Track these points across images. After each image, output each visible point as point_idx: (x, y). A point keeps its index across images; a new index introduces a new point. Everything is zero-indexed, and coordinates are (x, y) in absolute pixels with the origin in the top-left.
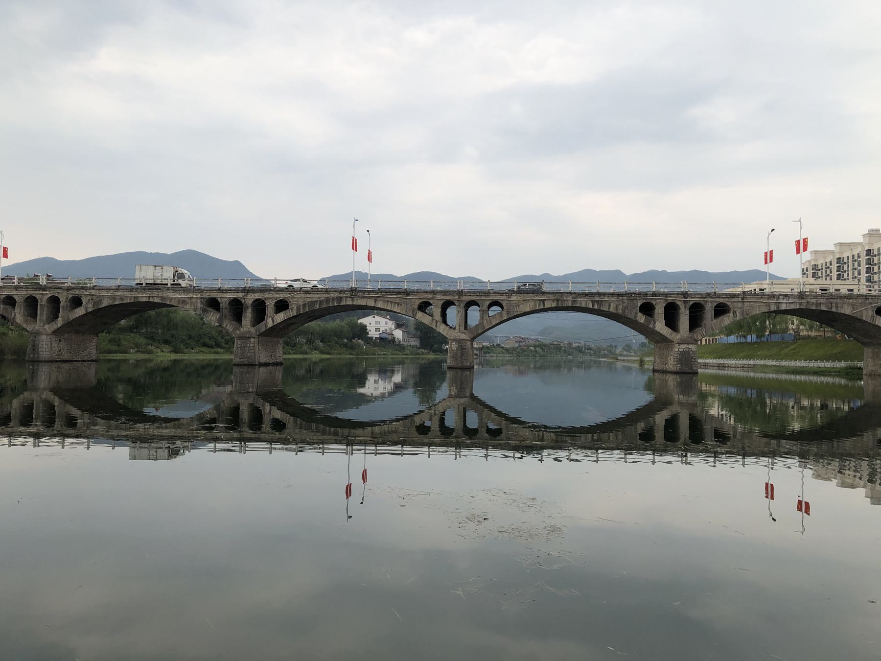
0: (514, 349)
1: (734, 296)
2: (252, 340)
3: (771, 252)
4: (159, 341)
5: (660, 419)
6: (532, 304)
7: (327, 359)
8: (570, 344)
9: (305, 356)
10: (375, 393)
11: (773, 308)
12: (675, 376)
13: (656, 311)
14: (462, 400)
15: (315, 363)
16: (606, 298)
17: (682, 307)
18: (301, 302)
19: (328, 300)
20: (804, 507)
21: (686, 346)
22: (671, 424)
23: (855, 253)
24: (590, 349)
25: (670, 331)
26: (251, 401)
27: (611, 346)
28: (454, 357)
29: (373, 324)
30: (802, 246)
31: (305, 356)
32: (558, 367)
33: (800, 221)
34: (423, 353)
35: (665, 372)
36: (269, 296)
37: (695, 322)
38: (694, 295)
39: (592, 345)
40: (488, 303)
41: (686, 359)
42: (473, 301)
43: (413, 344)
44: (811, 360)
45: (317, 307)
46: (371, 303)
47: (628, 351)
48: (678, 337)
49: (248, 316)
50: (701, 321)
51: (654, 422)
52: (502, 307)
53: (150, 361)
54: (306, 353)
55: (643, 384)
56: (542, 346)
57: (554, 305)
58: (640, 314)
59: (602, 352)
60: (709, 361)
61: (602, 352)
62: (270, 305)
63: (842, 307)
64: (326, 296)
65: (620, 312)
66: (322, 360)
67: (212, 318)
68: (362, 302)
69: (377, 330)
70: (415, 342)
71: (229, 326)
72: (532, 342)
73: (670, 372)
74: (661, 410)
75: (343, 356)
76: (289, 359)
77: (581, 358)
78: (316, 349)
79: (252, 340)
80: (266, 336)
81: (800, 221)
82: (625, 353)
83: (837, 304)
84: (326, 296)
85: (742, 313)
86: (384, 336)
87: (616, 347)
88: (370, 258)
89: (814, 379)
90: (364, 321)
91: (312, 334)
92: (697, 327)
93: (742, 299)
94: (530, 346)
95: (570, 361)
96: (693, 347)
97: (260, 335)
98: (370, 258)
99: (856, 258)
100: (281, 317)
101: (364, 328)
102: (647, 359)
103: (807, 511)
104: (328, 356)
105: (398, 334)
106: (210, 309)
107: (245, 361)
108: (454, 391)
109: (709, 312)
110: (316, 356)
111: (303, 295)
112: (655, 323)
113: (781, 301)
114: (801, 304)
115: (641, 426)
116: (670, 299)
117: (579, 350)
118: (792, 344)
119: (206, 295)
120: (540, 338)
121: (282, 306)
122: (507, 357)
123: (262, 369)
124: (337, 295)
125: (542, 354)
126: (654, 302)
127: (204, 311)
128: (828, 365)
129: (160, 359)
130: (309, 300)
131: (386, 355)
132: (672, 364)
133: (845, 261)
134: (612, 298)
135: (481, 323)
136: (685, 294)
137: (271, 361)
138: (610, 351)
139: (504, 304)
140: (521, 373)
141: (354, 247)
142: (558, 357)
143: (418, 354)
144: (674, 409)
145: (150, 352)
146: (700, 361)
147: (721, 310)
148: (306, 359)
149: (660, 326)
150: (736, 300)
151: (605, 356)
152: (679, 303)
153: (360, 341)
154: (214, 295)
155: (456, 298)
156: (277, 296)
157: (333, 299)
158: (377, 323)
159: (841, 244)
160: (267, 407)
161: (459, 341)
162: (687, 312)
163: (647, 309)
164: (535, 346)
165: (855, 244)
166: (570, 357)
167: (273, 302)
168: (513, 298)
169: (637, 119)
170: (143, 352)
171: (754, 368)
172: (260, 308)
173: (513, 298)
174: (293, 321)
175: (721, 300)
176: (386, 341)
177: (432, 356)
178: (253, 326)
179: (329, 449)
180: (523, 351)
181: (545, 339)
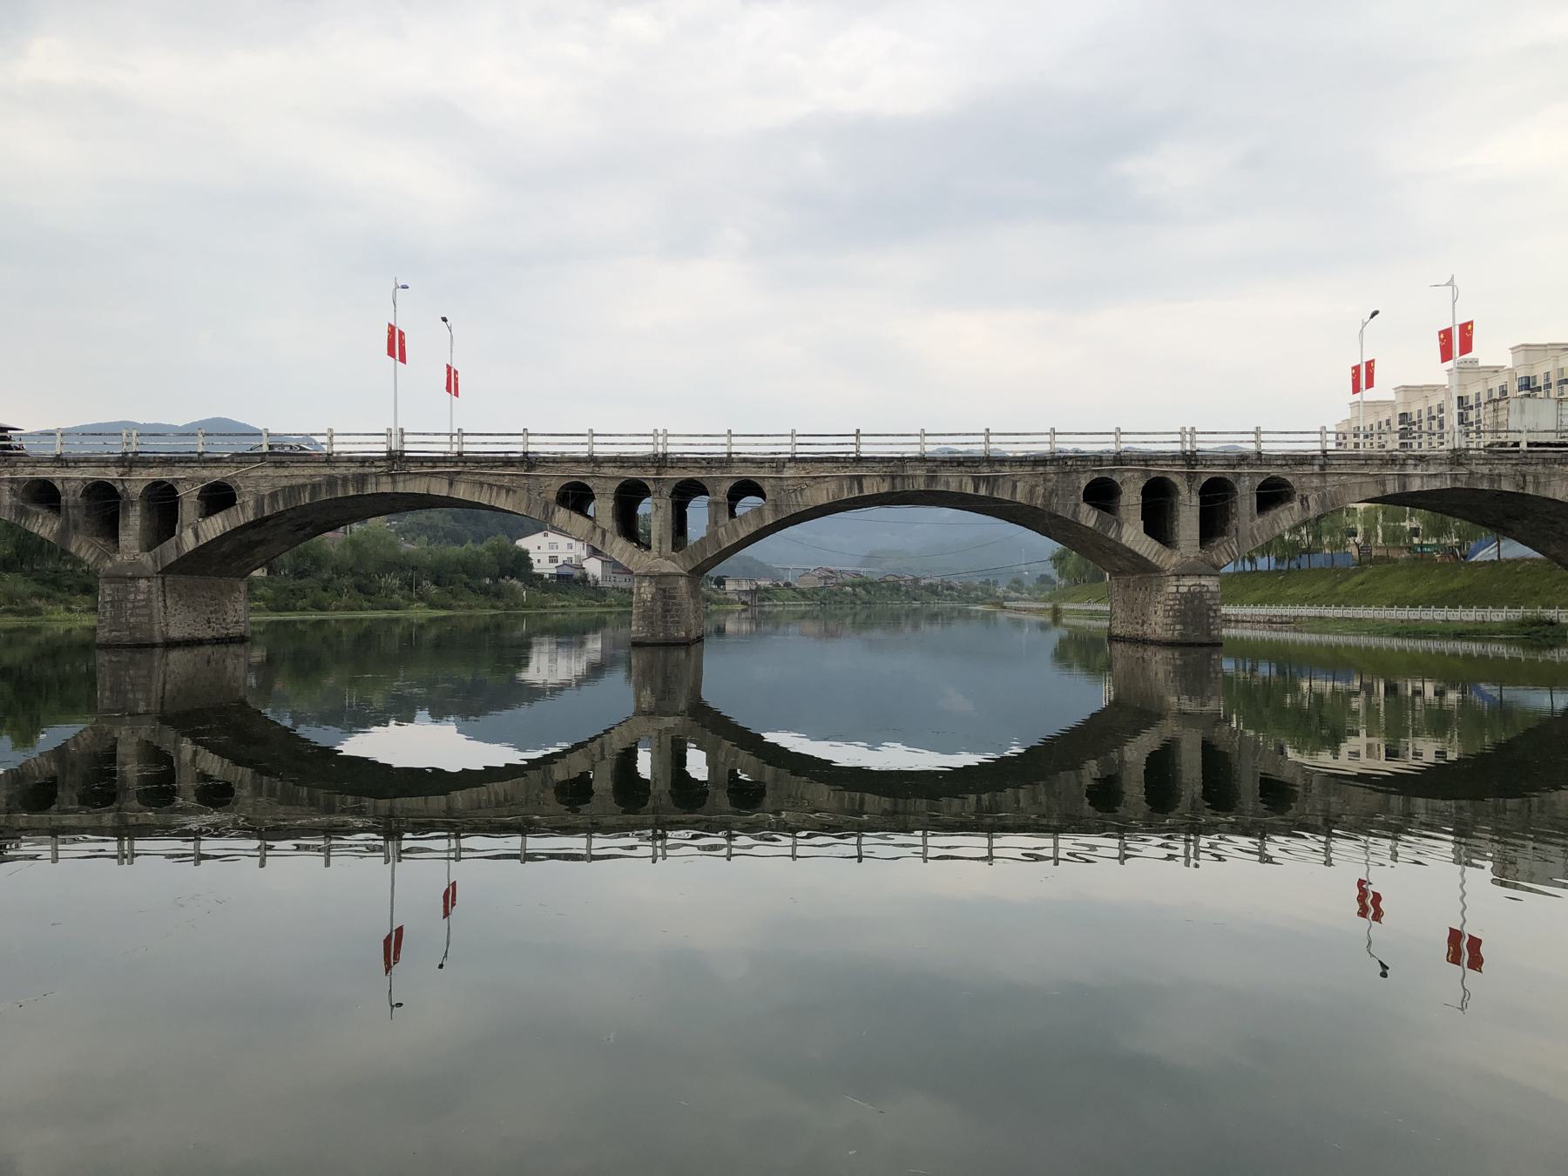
0: (815, 591)
1: (1301, 460)
2: (143, 584)
3: (1370, 365)
4: (70, 587)
5: (1136, 752)
6: (833, 486)
7: (444, 619)
8: (916, 580)
10: (553, 680)
11: (1392, 488)
12: (1168, 653)
13: (1124, 500)
14: (669, 722)
15: (421, 627)
16: (1006, 470)
17: (1183, 488)
18: (265, 489)
19: (331, 482)
20: (1464, 950)
21: (1195, 581)
22: (1161, 765)
23: (1434, 403)
24: (951, 588)
25: (1156, 545)
26: (144, 732)
27: (987, 582)
28: (647, 617)
29: (545, 548)
30: (1456, 341)
32: (895, 620)
33: (1451, 283)
35: (1143, 642)
36: (188, 473)
37: (1213, 524)
39: (955, 583)
40: (727, 485)
41: (1195, 610)
42: (691, 481)
44: (1402, 606)
45: (306, 499)
46: (440, 488)
47: (1017, 590)
48: (1174, 560)
49: (133, 524)
50: (1226, 521)
51: (1122, 762)
52: (760, 493)
53: (35, 630)
55: (1051, 650)
56: (866, 585)
57: (885, 488)
58: (1085, 507)
62: (189, 496)
63: (1548, 484)
64: (328, 471)
65: (1039, 503)
66: (432, 621)
67: (44, 526)
68: (418, 487)
69: (553, 559)
71: (84, 549)
72: (848, 579)
74: (1137, 733)
75: (477, 612)
76: (1302, 601)
77: (936, 605)
78: (421, 599)
79: (143, 584)
80: (181, 572)
81: (1451, 283)
82: (1013, 594)
83: (1536, 477)
84: (328, 471)
85: (1321, 502)
86: (566, 570)
87: (996, 583)
88: (452, 385)
89: (1449, 646)
90: (523, 543)
91: (414, 568)
92: (1223, 533)
93: (1322, 467)
96: (1211, 583)
97: (167, 570)
98: (452, 385)
99: (1435, 413)
100: (215, 526)
101: (523, 558)
102: (1065, 606)
103: (1476, 962)
104: (443, 613)
105: (594, 567)
106: (33, 508)
107: (125, 636)
108: (647, 699)
109: (1245, 500)
110: (418, 613)
111: (270, 471)
112: (1120, 526)
113: (1410, 470)
114: (1455, 478)
115: (1092, 770)
116: (1156, 471)
117: (932, 590)
118: (1356, 572)
119: (25, 473)
120: (862, 570)
121: (218, 498)
122: (803, 606)
123: (175, 655)
124: (355, 470)
125: (866, 598)
126: (1116, 478)
127: (22, 512)
128: (1472, 615)
129: (61, 628)
130: (285, 482)
131: (567, 608)
132: (1159, 623)
133: (1415, 418)
134: (1019, 470)
135: (712, 535)
137: (209, 634)
139: (766, 489)
140: (830, 635)
141: (396, 345)
142: (896, 605)
145: (36, 612)
146: (1224, 610)
147: (1272, 494)
148: (397, 621)
149: (1133, 535)
150: (1307, 469)
151: (977, 601)
152: (1175, 479)
153: (514, 582)
154: (44, 473)
156: (205, 473)
157: (345, 479)
158: (552, 545)
159: (1406, 388)
160: (187, 747)
161: (658, 578)
162: (1196, 500)
163: (1102, 494)
164: (853, 586)
165: (1434, 388)
166: (916, 604)
167: (195, 491)
168: (787, 473)
169: (1022, 171)
170: (19, 613)
171: (1294, 623)
172: (163, 501)
173: (787, 473)
174: (254, 535)
175: (1274, 471)
176: (569, 581)
178: (149, 548)
179: (338, 846)
181: (873, 572)
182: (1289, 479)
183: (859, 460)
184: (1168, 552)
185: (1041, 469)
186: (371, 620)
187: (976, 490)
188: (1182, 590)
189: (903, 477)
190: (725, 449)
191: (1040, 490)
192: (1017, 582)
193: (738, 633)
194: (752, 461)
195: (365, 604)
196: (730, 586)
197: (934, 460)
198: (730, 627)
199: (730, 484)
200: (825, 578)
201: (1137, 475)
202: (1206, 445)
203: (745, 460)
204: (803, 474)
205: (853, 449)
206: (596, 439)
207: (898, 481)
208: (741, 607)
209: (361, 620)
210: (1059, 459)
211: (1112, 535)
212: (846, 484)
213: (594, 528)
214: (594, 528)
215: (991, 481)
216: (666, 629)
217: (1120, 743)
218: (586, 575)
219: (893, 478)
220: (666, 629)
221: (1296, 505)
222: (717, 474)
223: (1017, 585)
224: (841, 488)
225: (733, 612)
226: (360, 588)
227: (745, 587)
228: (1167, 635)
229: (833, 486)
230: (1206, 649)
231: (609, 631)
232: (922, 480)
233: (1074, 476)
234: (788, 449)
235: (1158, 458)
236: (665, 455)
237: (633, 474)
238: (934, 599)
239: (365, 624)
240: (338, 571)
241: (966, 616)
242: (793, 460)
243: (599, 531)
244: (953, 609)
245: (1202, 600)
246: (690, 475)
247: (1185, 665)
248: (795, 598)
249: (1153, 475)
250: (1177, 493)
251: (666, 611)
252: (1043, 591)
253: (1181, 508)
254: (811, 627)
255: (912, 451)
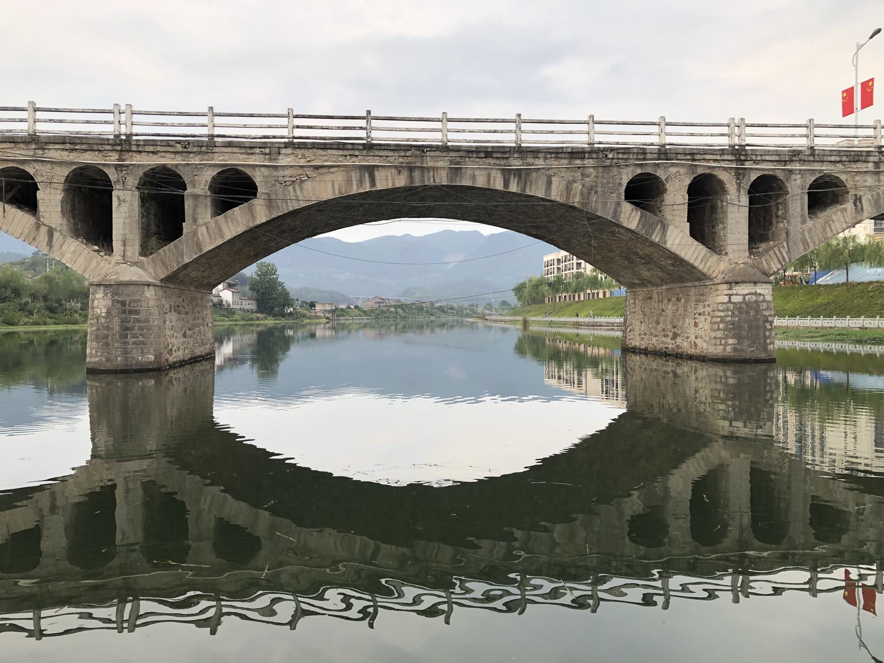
0: (373, 311)
1: (857, 157)
8: (432, 304)
9: (76, 327)
12: (719, 371)
16: (540, 163)
22: (707, 489)
24: (452, 308)
27: (472, 305)
31: (76, 327)
32: (421, 327)
34: (258, 319)
37: (760, 230)
38: (759, 155)
39: (455, 305)
41: (748, 322)
43: (248, 307)
44: (783, 316)
51: (666, 489)
54: (75, 323)
55: (513, 346)
56: (403, 306)
58: (627, 207)
59: (465, 312)
60: (553, 319)
61: (465, 312)
65: (576, 201)
70: (251, 305)
72: (393, 303)
73: (703, 359)
77: (443, 318)
82: (487, 312)
94: (391, 306)
95: (432, 321)
96: (765, 291)
112: (664, 228)
117: (442, 309)
122: (365, 320)
125: (403, 315)
126: (661, 174)
134: (554, 163)
136: (739, 153)
138: (472, 310)
142: (421, 319)
143: (252, 319)
144: (718, 453)
147: (824, 195)
149: (678, 238)
150: (862, 167)
151: (467, 316)
152: (723, 176)
155: (113, 158)
161: (115, 288)
162: (745, 200)
163: (644, 192)
164: (396, 307)
166: (433, 318)
168: (283, 161)
173: (283, 161)
175: (827, 168)
177: (270, 322)
180: (383, 312)
181: (407, 300)
182: (843, 177)
183: (370, 147)
184: (715, 257)
185: (578, 162)
186: (55, 331)
187: (506, 184)
188: (734, 299)
189: (422, 168)
190: (204, 131)
191: (578, 187)
192: (489, 305)
193: (324, 337)
194: (240, 146)
195: (48, 320)
196: (318, 307)
197: (458, 149)
198: (319, 333)
199: (214, 172)
200: (379, 303)
201: (682, 171)
202: (755, 139)
203: (230, 145)
204: (302, 162)
205: (362, 134)
206: (40, 115)
207: (417, 174)
208: (325, 321)
209: (45, 332)
210: (599, 150)
211: (656, 238)
212: (355, 176)
213: (38, 226)
214: (38, 226)
215: (522, 175)
216: (126, 352)
217: (664, 472)
218: (222, 301)
219: (411, 169)
220: (126, 352)
221: (849, 206)
222: (195, 160)
223: (489, 306)
224: (349, 181)
225: (320, 324)
226: (51, 310)
227: (328, 308)
228: (717, 350)
229: (339, 177)
230: (763, 367)
231: (238, 337)
232: (444, 173)
233: (615, 171)
234: (284, 132)
235: (706, 152)
236: (129, 136)
237: (88, 158)
238: (443, 315)
239: (48, 335)
240: (34, 297)
241: (461, 325)
242: (293, 145)
243: (44, 230)
244: (453, 321)
245: (758, 311)
246: (162, 161)
247: (739, 385)
248: (360, 315)
249: (700, 171)
250: (724, 191)
251: (125, 329)
252: (503, 310)
253: (730, 209)
254: (371, 333)
255: (433, 138)
